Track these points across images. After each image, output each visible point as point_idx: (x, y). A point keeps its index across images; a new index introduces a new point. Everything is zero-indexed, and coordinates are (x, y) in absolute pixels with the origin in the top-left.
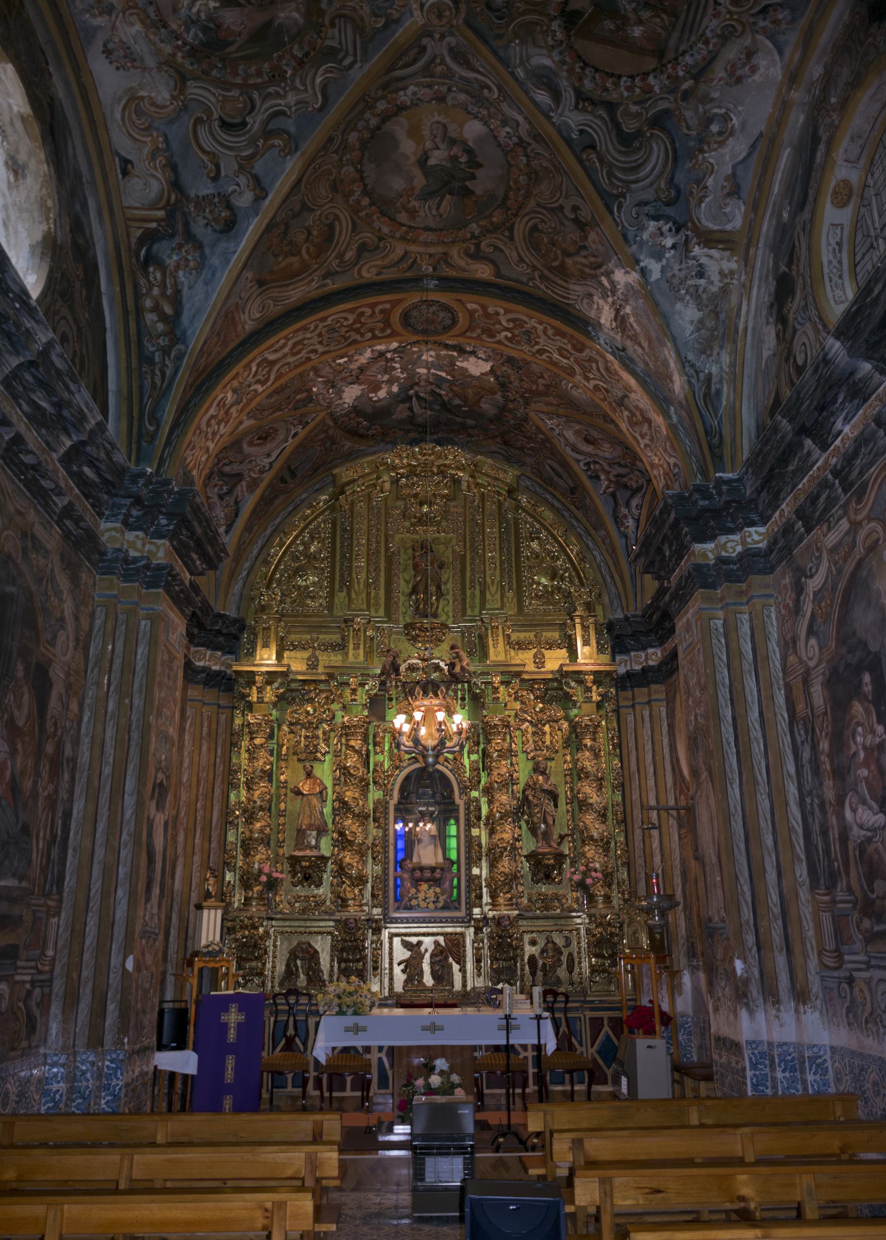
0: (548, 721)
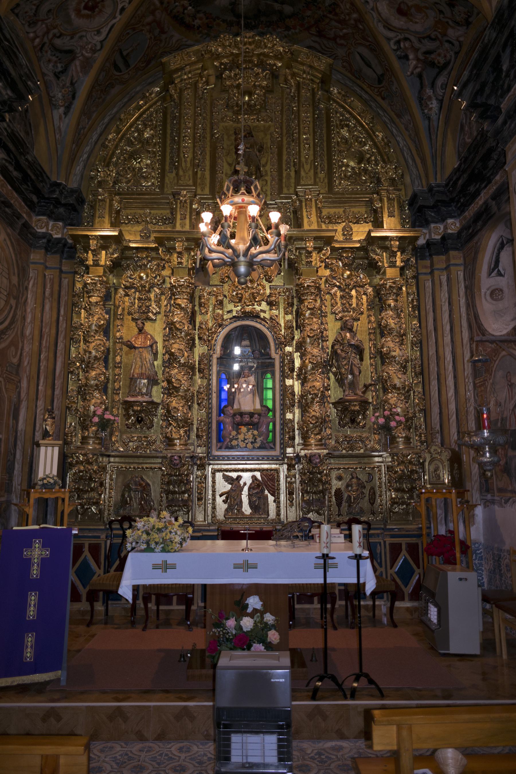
0: (354, 287)
